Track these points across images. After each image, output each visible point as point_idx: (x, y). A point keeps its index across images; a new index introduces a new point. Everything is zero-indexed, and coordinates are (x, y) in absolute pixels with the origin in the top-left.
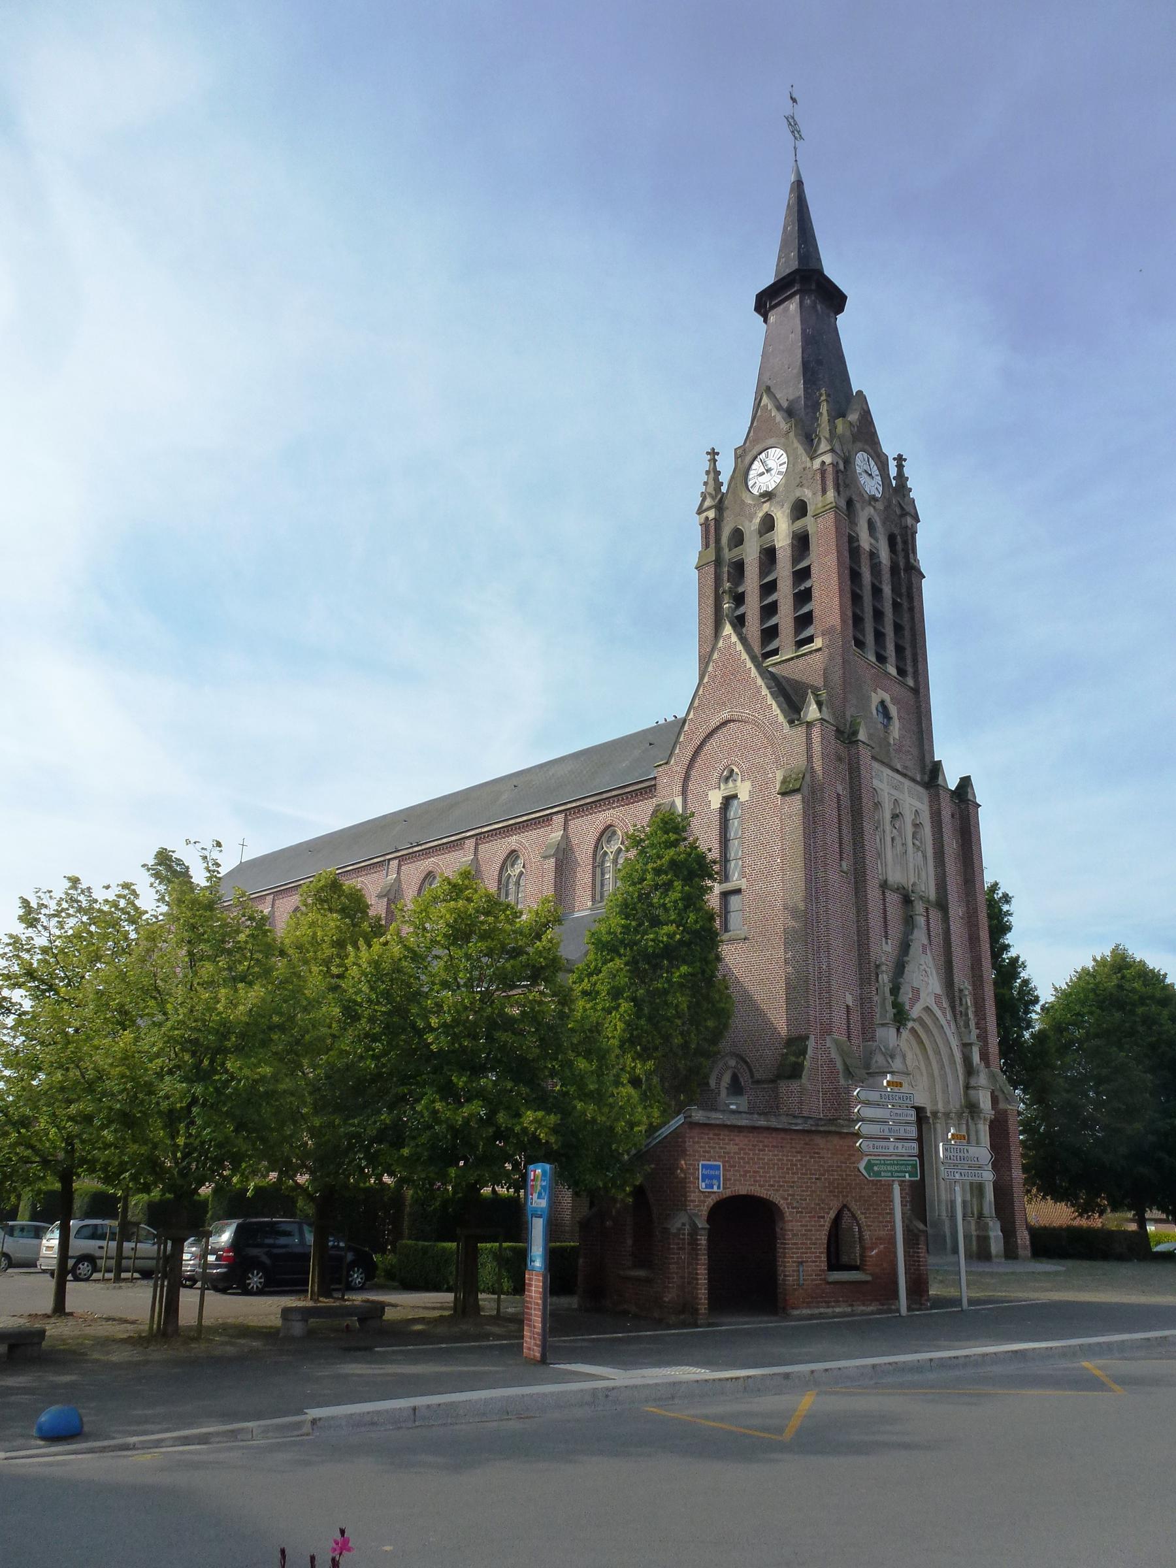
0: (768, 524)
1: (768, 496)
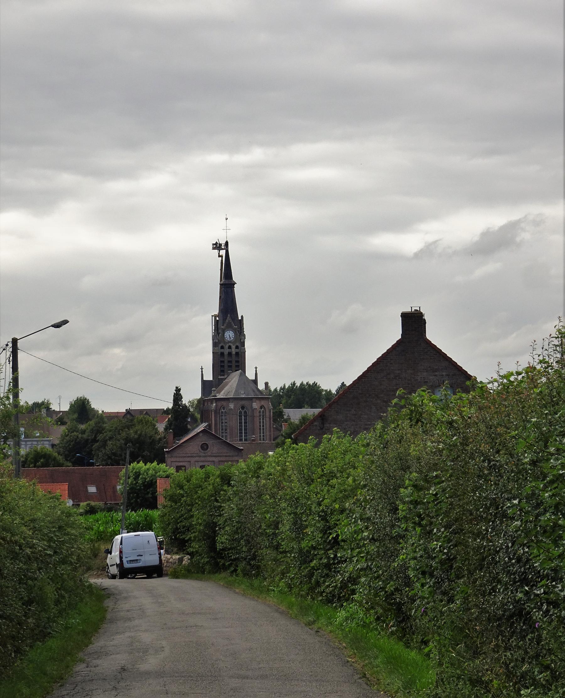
0: (230, 347)
1: (229, 342)
